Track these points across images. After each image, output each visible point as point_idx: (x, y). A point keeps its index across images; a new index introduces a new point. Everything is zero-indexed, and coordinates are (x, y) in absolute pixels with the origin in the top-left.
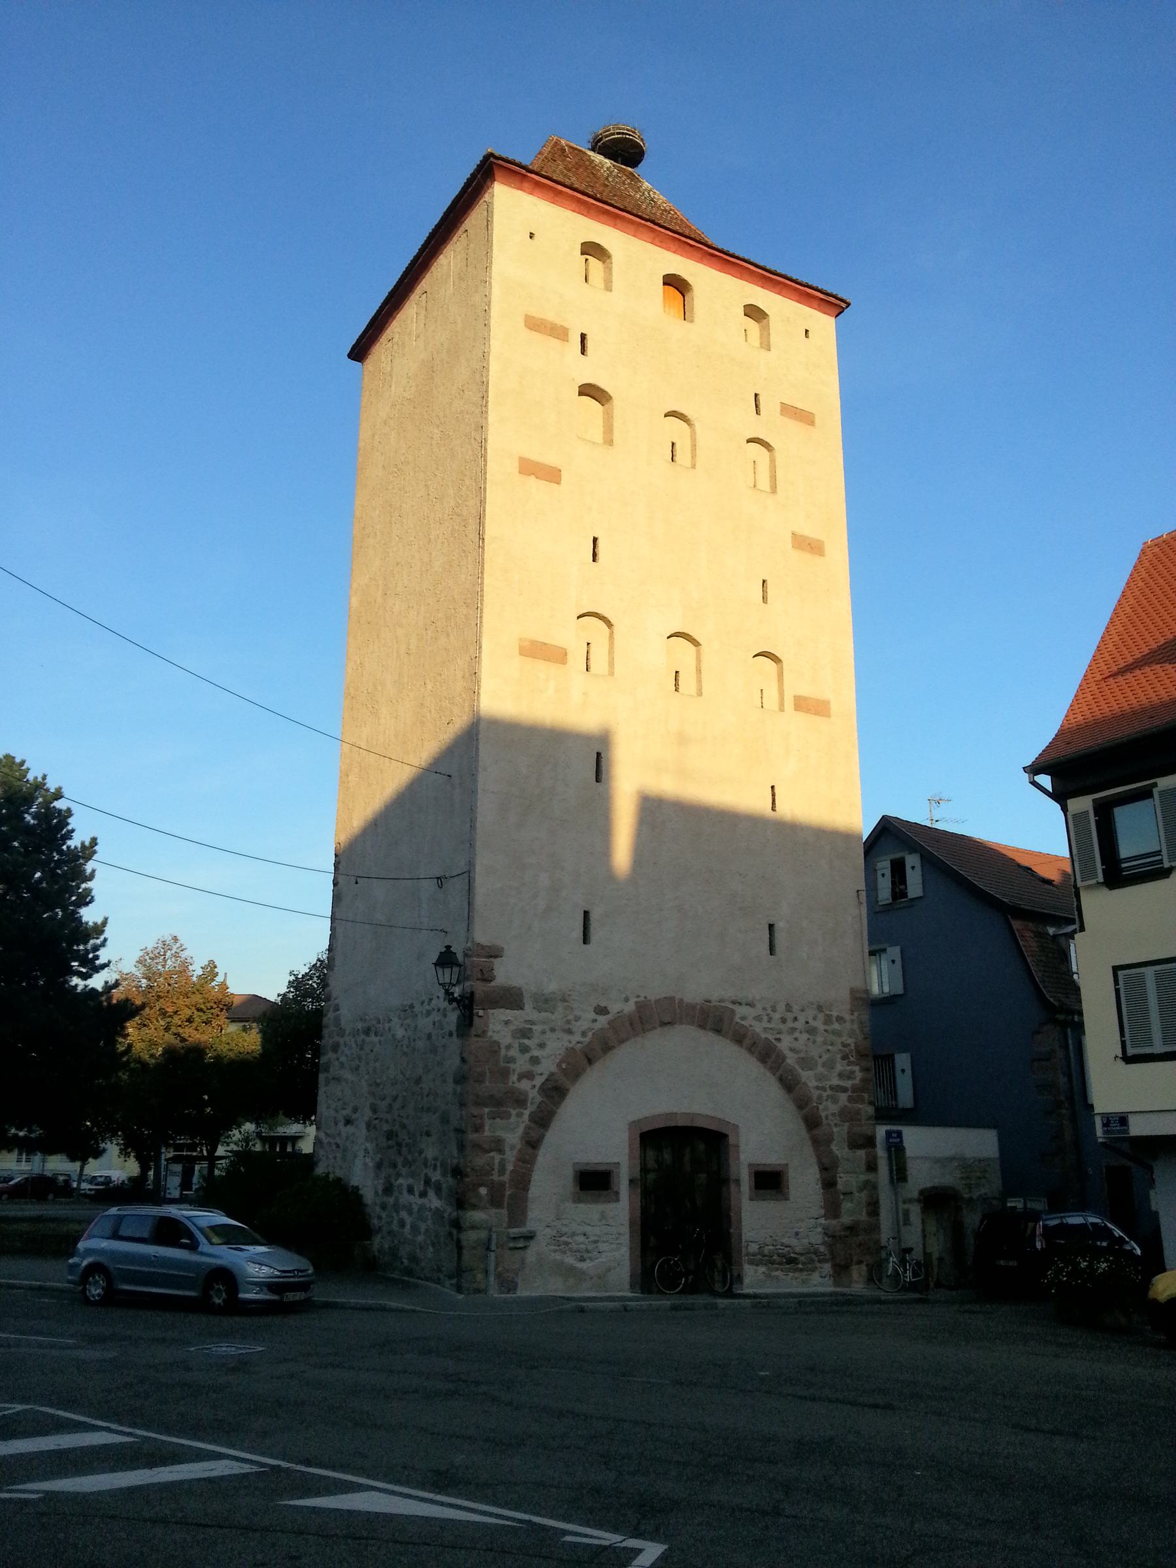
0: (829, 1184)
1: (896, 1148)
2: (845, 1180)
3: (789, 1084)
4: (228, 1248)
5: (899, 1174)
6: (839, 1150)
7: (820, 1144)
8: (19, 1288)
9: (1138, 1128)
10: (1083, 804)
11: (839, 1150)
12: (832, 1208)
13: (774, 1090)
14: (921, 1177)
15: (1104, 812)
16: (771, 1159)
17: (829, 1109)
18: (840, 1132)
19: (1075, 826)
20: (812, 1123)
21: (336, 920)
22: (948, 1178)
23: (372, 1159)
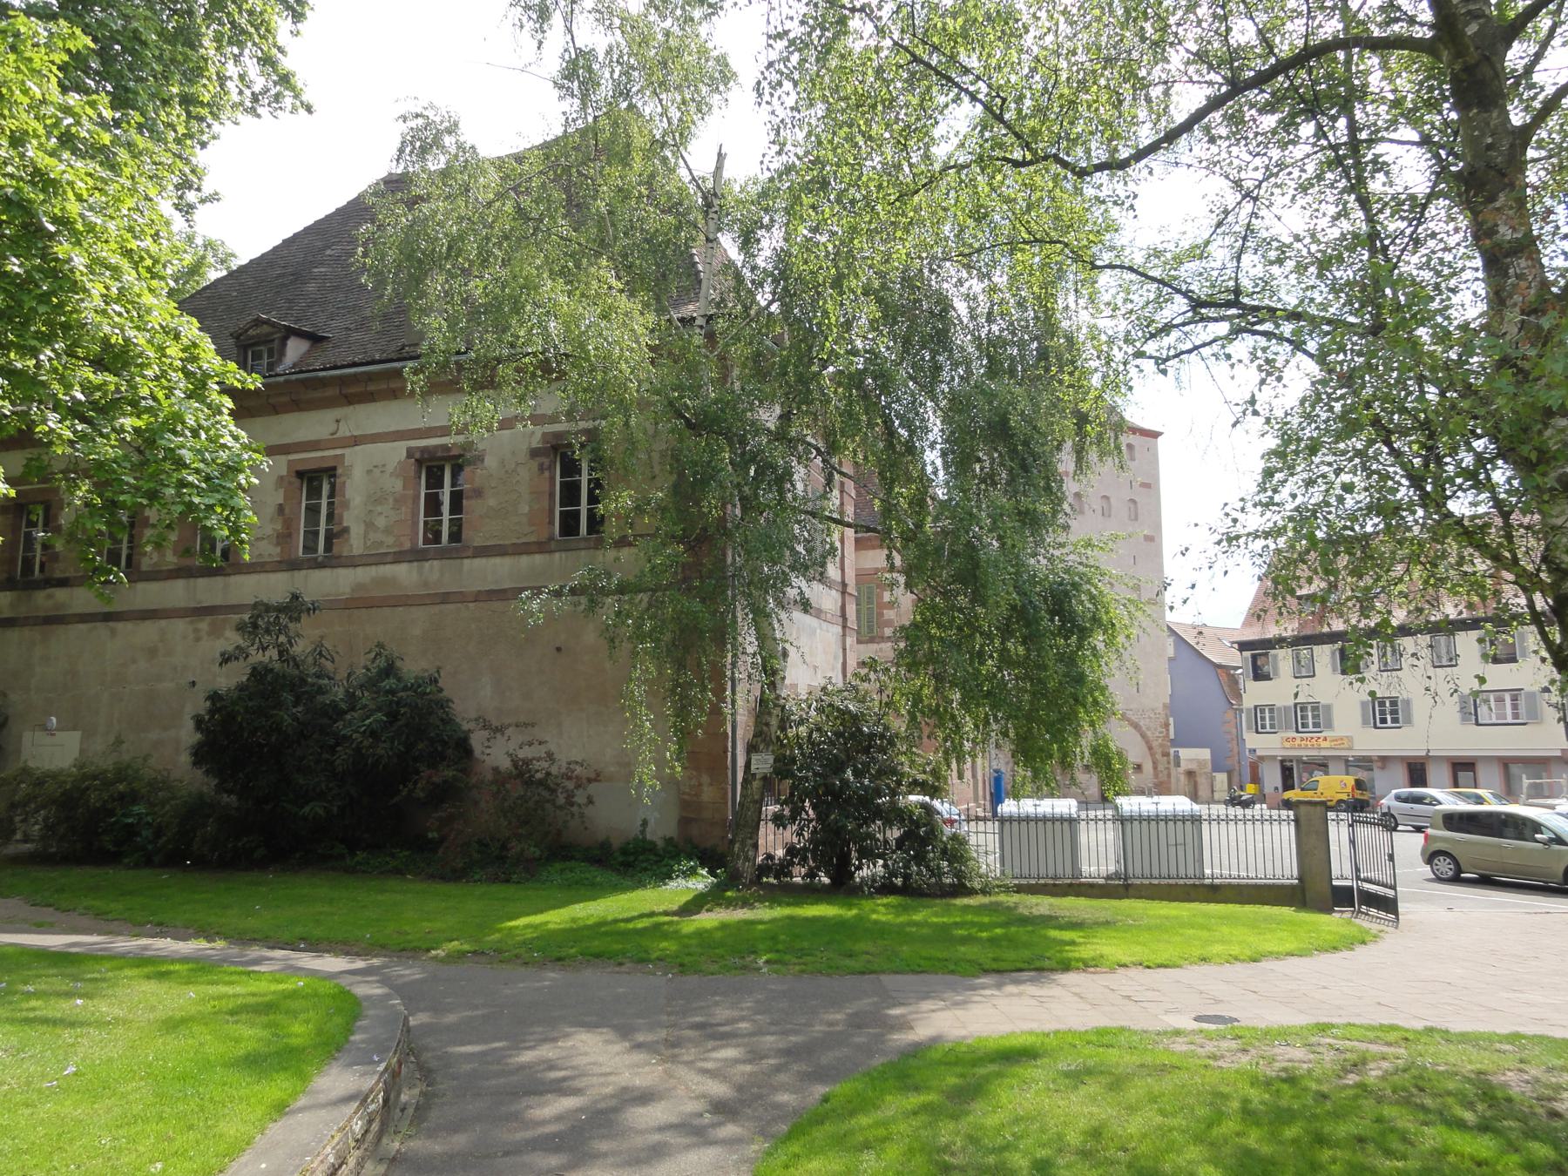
0: (1155, 768)
1: (1177, 757)
2: (1161, 767)
3: (1143, 736)
4: (1132, 459)
5: (1178, 764)
6: (1159, 756)
7: (1153, 755)
8: (173, 961)
9: (1259, 753)
10: (1247, 654)
11: (1159, 756)
12: (1156, 775)
13: (1139, 738)
14: (1184, 766)
15: (1254, 657)
16: (1138, 761)
17: (1155, 744)
18: (1159, 751)
19: (1244, 660)
20: (1150, 748)
21: (695, 174)
22: (1193, 766)
23: (952, 822)
